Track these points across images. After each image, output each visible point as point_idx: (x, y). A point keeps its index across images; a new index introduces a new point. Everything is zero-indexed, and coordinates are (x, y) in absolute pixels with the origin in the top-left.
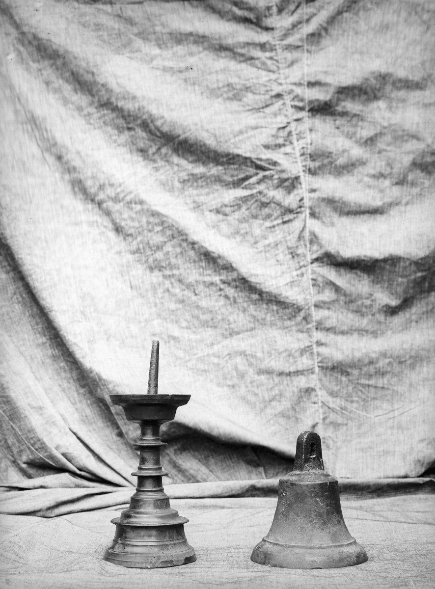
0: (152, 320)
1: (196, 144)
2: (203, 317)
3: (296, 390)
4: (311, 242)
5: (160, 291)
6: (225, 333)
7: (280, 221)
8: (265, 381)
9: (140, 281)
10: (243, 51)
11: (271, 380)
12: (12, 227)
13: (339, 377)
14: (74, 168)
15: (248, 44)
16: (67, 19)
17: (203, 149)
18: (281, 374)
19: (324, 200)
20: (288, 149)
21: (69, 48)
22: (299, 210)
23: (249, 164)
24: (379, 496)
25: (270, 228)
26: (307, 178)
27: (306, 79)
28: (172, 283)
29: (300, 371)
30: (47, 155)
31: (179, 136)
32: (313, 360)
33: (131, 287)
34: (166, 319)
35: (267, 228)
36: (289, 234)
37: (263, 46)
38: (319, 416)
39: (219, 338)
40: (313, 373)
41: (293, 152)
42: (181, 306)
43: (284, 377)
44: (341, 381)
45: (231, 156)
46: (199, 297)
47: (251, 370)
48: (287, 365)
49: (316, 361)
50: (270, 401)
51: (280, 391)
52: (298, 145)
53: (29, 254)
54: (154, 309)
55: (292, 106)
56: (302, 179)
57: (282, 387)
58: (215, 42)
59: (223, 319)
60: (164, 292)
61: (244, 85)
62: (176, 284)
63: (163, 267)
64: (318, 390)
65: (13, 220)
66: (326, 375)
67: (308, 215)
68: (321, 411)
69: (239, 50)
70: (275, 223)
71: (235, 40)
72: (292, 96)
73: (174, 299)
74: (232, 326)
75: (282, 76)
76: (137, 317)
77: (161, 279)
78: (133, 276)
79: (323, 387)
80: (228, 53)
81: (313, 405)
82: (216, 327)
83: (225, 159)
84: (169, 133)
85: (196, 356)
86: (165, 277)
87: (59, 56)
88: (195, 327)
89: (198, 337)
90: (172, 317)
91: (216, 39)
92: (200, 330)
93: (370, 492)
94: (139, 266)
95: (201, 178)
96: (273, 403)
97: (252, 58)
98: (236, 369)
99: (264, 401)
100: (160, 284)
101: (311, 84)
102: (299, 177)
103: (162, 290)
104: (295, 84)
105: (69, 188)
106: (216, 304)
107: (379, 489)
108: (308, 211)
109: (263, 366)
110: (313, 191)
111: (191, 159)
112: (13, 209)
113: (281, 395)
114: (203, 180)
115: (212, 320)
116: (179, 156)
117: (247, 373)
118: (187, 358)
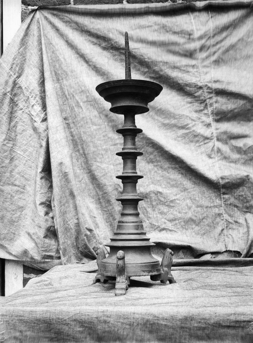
0: (150, 185)
1: (165, 110)
2: (171, 183)
3: (213, 214)
4: (218, 152)
5: (153, 172)
6: (182, 189)
7: (202, 143)
8: (200, 210)
9: (144, 168)
10: (184, 69)
11: (203, 210)
12: (88, 150)
13: (233, 208)
14: (113, 120)
15: (187, 66)
16: (108, 58)
17: (168, 112)
18: (207, 207)
19: (222, 133)
20: (206, 111)
21: (109, 71)
22: (211, 138)
23: (188, 119)
24: (245, 266)
25: (198, 146)
26: (214, 124)
27: (213, 80)
28: (158, 169)
29: (216, 206)
30: (101, 115)
31: (157, 107)
32: (221, 201)
33: (140, 171)
34: (155, 184)
35: (197, 146)
36: (207, 149)
37: (193, 66)
38: (224, 226)
39: (179, 192)
40: (221, 207)
41: (208, 113)
42: (162, 178)
43: (208, 209)
44: (234, 210)
45: (180, 115)
46: (170, 174)
47: (194, 206)
48: (210, 203)
49: (223, 201)
50: (203, 219)
51: (207, 214)
52: (210, 109)
53: (95, 161)
54: (150, 180)
55: (207, 92)
56: (212, 124)
57: (207, 213)
58: (172, 65)
59: (181, 184)
60: (154, 173)
61: (185, 84)
62: (160, 169)
63: (153, 162)
64: (224, 214)
65: (88, 147)
66: (227, 207)
67: (215, 140)
68: (225, 223)
69: (182, 68)
70: (201, 144)
71: (181, 64)
72: (206, 88)
73: (159, 175)
74: (185, 186)
75: (202, 79)
76: (143, 184)
77: (153, 167)
78: (141, 166)
79: (226, 212)
80: (177, 70)
81: (222, 221)
82: (178, 187)
83: (178, 117)
84: (153, 106)
85: (169, 200)
86: (154, 166)
87: (105, 74)
88: (168, 187)
89: (170, 192)
90: (158, 183)
91: (172, 64)
92: (171, 189)
93: (241, 264)
94: (143, 162)
95: (167, 125)
96: (204, 220)
97: (188, 72)
98: (187, 205)
99: (200, 219)
100: (152, 169)
101: (215, 82)
102: (211, 124)
103: (153, 172)
104: (208, 82)
105: (111, 129)
106: (178, 177)
107: (246, 263)
108: (215, 139)
109: (199, 204)
110: (217, 129)
111: (163, 117)
112: (88, 142)
113: (207, 217)
114: (168, 126)
115: (176, 184)
116: (157, 116)
117: (192, 207)
118: (166, 201)
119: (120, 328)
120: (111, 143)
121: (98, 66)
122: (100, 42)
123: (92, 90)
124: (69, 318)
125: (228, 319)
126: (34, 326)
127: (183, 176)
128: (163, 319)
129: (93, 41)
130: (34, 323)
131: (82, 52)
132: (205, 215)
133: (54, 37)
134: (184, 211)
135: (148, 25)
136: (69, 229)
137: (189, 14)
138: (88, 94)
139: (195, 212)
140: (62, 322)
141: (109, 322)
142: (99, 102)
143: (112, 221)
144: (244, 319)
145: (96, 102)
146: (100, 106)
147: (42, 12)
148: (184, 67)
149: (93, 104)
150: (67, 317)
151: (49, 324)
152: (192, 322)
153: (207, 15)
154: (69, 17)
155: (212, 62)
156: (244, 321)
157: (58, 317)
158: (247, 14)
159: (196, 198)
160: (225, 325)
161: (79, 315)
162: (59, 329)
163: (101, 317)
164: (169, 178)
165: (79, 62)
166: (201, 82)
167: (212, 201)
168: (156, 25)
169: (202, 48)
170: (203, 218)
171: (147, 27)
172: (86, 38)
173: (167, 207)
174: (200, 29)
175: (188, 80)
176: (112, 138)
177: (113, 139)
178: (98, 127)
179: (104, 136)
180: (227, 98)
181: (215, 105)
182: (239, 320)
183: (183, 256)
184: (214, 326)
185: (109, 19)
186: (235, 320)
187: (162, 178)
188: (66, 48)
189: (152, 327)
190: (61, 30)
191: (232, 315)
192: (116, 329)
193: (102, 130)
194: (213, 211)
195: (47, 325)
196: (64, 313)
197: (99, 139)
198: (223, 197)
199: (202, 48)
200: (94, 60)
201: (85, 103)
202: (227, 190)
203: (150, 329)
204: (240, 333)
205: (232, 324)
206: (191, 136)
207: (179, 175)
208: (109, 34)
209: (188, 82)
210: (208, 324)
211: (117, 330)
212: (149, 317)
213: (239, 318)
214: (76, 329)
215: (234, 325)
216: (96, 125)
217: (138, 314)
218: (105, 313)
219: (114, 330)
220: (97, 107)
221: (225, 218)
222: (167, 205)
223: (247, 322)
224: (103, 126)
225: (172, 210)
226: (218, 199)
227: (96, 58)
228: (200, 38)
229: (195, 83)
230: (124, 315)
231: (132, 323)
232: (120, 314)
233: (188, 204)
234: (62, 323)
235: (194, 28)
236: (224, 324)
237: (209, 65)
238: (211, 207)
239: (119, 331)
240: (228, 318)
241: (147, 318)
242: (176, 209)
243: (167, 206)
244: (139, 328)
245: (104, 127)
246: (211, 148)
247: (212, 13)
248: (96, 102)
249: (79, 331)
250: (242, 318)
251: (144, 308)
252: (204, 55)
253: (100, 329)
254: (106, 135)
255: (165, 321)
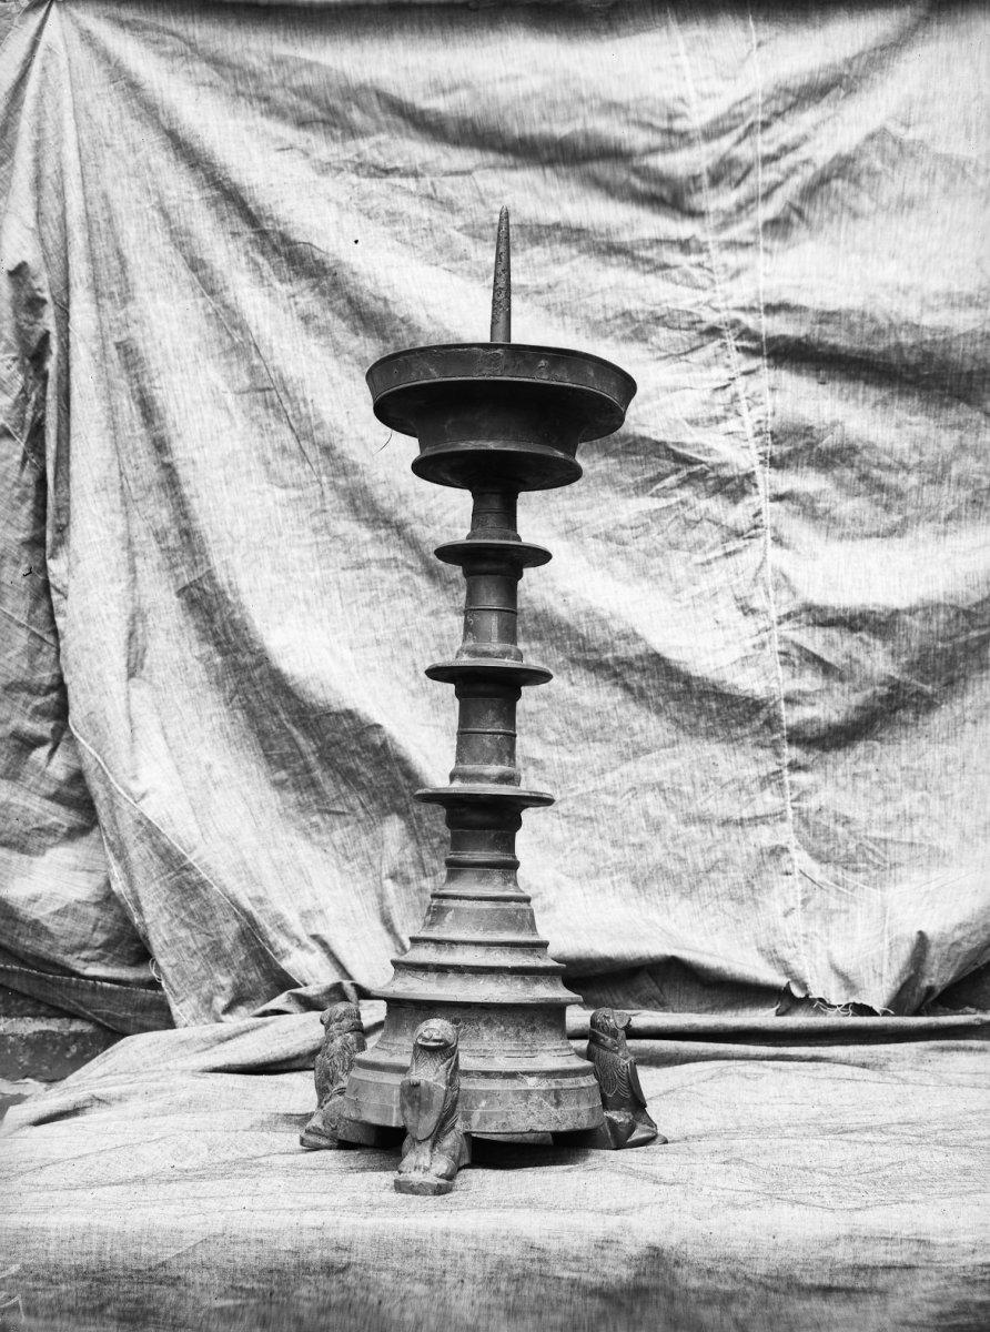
3: (752, 850)
8: (698, 836)
10: (649, 254)
18: (725, 823)
20: (732, 425)
21: (345, 259)
27: (764, 300)
37: (684, 246)
40: (783, 820)
41: (740, 429)
43: (731, 828)
45: (631, 441)
46: (576, 688)
47: (672, 816)
48: (737, 807)
49: (789, 798)
51: (724, 852)
55: (737, 349)
56: (759, 478)
57: (727, 846)
58: (599, 239)
67: (770, 542)
68: (799, 887)
69: (643, 253)
74: (638, 738)
80: (622, 258)
82: (608, 741)
87: (325, 271)
88: (571, 741)
89: (578, 759)
91: (602, 235)
92: (581, 746)
96: (713, 875)
97: (665, 266)
98: (646, 814)
101: (771, 309)
102: (754, 473)
104: (743, 309)
106: (609, 700)
109: (693, 810)
119: (387, 1294)
120: (342, 557)
121: (297, 236)
122: (308, 141)
123: (274, 344)
124: (178, 1255)
125: (824, 1261)
126: (35, 1290)
127: (630, 697)
128: (563, 1257)
129: (281, 134)
130: (37, 1278)
131: (235, 177)
132: (719, 855)
133: (122, 117)
134: (634, 840)
135: (504, 74)
136: (195, 888)
137: (669, 33)
138: (256, 362)
139: (679, 841)
140: (156, 1275)
141: (344, 1270)
142: (299, 395)
143: (372, 852)
144: (889, 1259)
145: (287, 393)
146: (303, 410)
147: (74, 11)
148: (647, 248)
149: (276, 400)
150: (173, 1252)
151: (98, 1280)
152: (679, 1270)
153: (741, 34)
154: (185, 33)
155: (760, 226)
156: (888, 1268)
157: (134, 1251)
158: (901, 35)
159: (680, 785)
160: (812, 1285)
161: (221, 1240)
162: (137, 1301)
163: (312, 1248)
164: (576, 704)
165: (223, 219)
166: (717, 310)
167: (745, 798)
168: (536, 71)
169: (722, 173)
170: (709, 867)
171: (501, 80)
172: (252, 123)
173: (564, 822)
174: (711, 96)
175: (662, 298)
176: (349, 538)
177: (351, 544)
178: (294, 493)
179: (315, 530)
180: (817, 376)
181: (770, 402)
182: (870, 1263)
183: (657, 990)
184: (767, 1288)
185: (347, 43)
186: (851, 1262)
187: (546, 705)
188: (169, 160)
189: (517, 1290)
190: (147, 86)
191: (843, 1242)
192: (373, 1299)
193: (310, 507)
194: (752, 839)
195: (91, 1287)
196: (159, 1235)
197: (297, 540)
198: (791, 782)
199: (722, 173)
200: (280, 212)
201: (246, 396)
202: (807, 753)
203: (511, 1299)
204: (873, 1318)
205: (841, 1280)
206: (675, 524)
207: (615, 695)
208: (351, 110)
209: (664, 305)
210: (746, 1278)
211: (376, 1301)
212: (509, 1252)
213: (868, 1254)
214: (206, 1303)
215: (849, 1285)
216: (285, 487)
217: (458, 1236)
218: (330, 1235)
219: (364, 1302)
220: (290, 413)
221: (796, 863)
222: (566, 813)
223: (901, 1268)
224: (314, 489)
225: (584, 832)
226: (769, 790)
227: (288, 205)
228: (713, 132)
229: (690, 314)
230: (406, 1242)
231: (438, 1273)
232: (391, 1238)
233: (651, 811)
234: (150, 1277)
235: (689, 90)
236: (808, 1281)
237: (751, 238)
238: (741, 824)
239: (386, 1306)
240: (825, 1253)
241: (498, 1252)
242: (602, 829)
243: (565, 816)
244: (465, 1292)
245: (318, 493)
246: (752, 571)
247: (760, 25)
248: (287, 393)
249: (221, 1310)
250: (878, 1254)
251: (485, 1214)
252: (728, 198)
253: (309, 1299)
254: (327, 525)
255: (573, 1265)
